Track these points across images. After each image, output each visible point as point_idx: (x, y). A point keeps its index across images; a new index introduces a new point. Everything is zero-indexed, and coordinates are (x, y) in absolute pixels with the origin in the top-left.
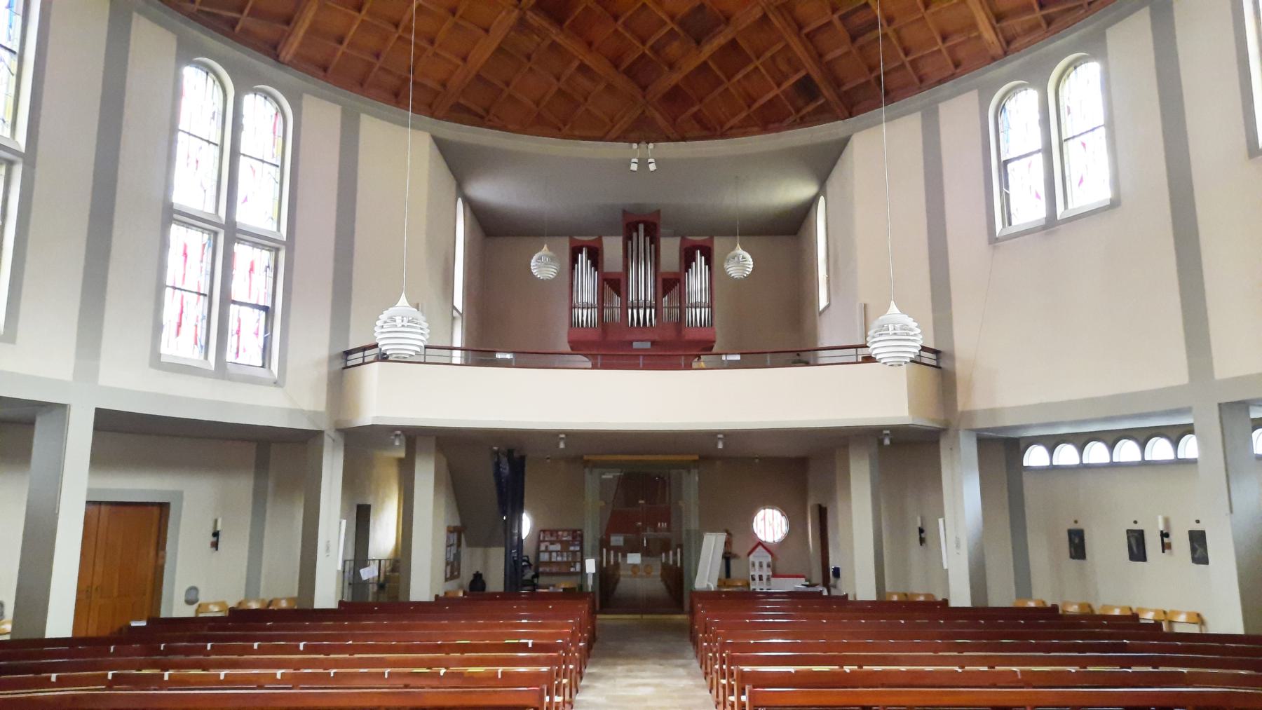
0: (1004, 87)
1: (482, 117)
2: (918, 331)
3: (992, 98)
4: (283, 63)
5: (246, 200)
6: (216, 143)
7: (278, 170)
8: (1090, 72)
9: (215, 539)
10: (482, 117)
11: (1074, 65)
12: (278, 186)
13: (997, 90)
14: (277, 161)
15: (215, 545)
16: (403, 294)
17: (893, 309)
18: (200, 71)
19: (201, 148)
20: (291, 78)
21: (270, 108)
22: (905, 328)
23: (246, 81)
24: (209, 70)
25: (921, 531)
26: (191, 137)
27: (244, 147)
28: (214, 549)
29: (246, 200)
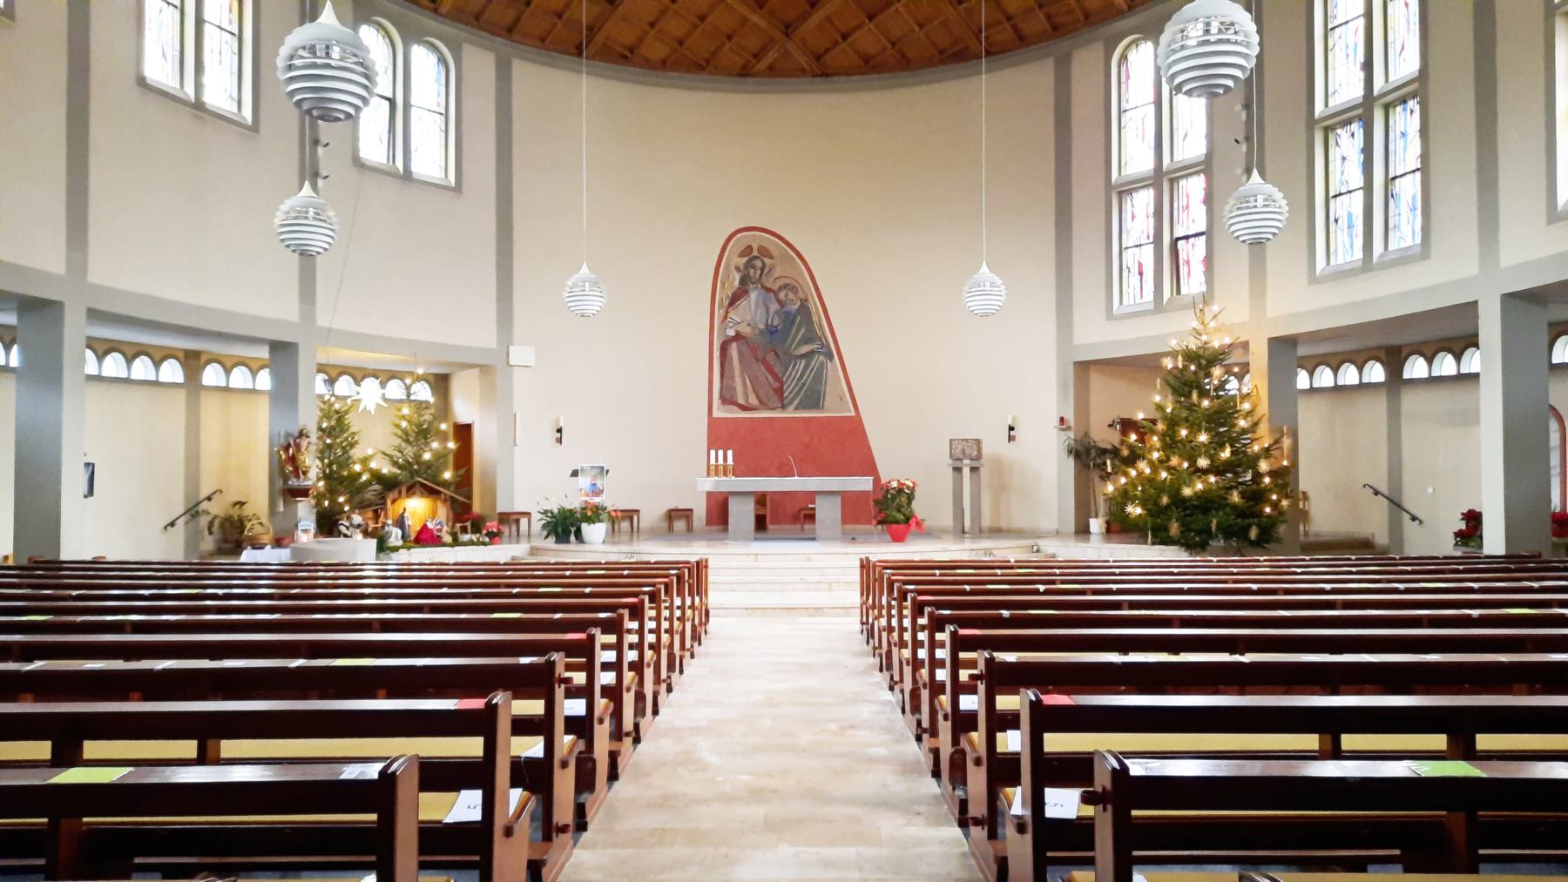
0: (1120, 46)
1: (625, 57)
2: (1004, 287)
3: (1115, 48)
4: (441, 15)
5: (416, 150)
6: (175, 4)
7: (443, 118)
8: (1147, 48)
9: (559, 435)
10: (625, 57)
11: (1135, 42)
12: (443, 135)
13: (1119, 43)
14: (230, 23)
15: (560, 441)
16: (585, 264)
17: (984, 269)
18: (371, 28)
19: (161, 11)
20: (451, 29)
21: (432, 59)
22: (993, 285)
23: (412, 35)
24: (380, 27)
25: (1011, 428)
26: (223, 32)
27: (413, 101)
28: (559, 444)
29: (416, 150)
